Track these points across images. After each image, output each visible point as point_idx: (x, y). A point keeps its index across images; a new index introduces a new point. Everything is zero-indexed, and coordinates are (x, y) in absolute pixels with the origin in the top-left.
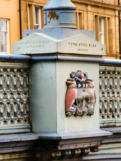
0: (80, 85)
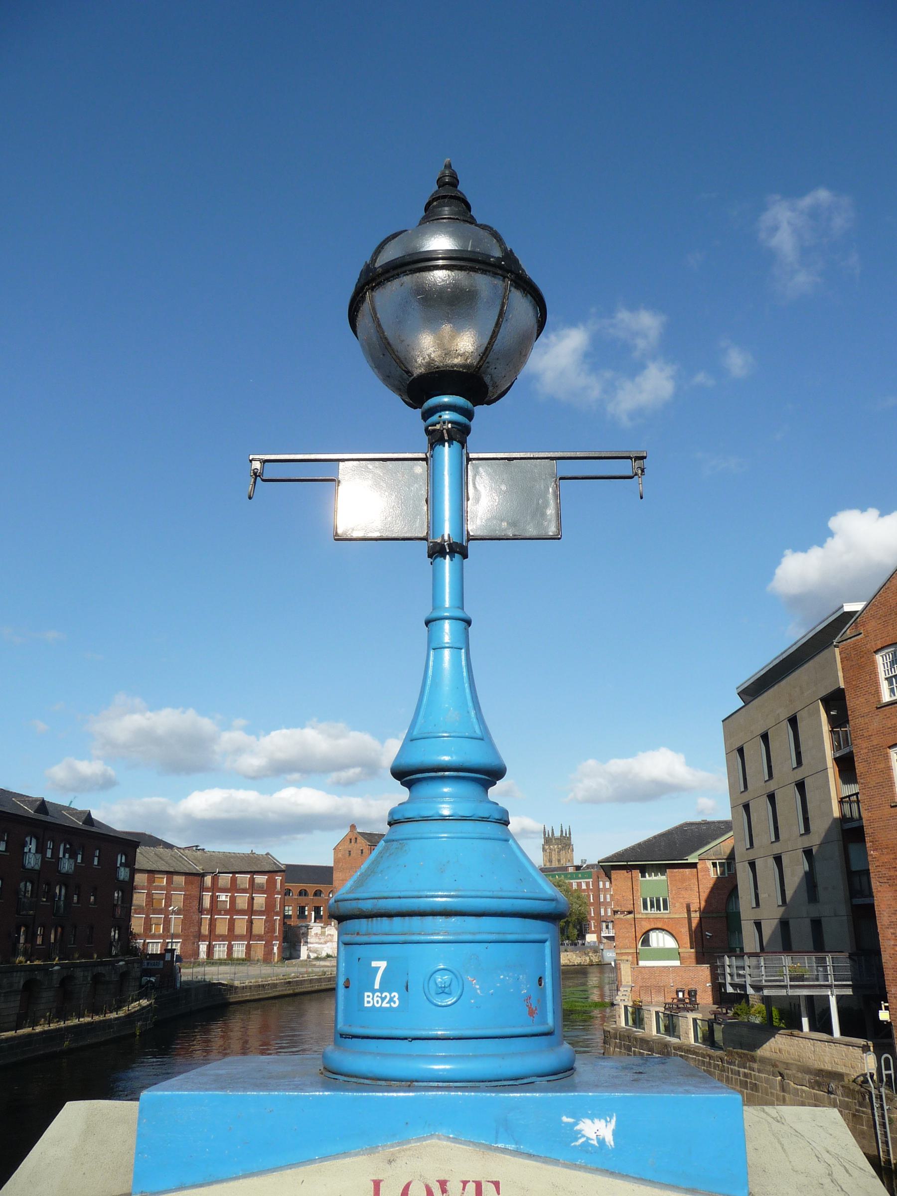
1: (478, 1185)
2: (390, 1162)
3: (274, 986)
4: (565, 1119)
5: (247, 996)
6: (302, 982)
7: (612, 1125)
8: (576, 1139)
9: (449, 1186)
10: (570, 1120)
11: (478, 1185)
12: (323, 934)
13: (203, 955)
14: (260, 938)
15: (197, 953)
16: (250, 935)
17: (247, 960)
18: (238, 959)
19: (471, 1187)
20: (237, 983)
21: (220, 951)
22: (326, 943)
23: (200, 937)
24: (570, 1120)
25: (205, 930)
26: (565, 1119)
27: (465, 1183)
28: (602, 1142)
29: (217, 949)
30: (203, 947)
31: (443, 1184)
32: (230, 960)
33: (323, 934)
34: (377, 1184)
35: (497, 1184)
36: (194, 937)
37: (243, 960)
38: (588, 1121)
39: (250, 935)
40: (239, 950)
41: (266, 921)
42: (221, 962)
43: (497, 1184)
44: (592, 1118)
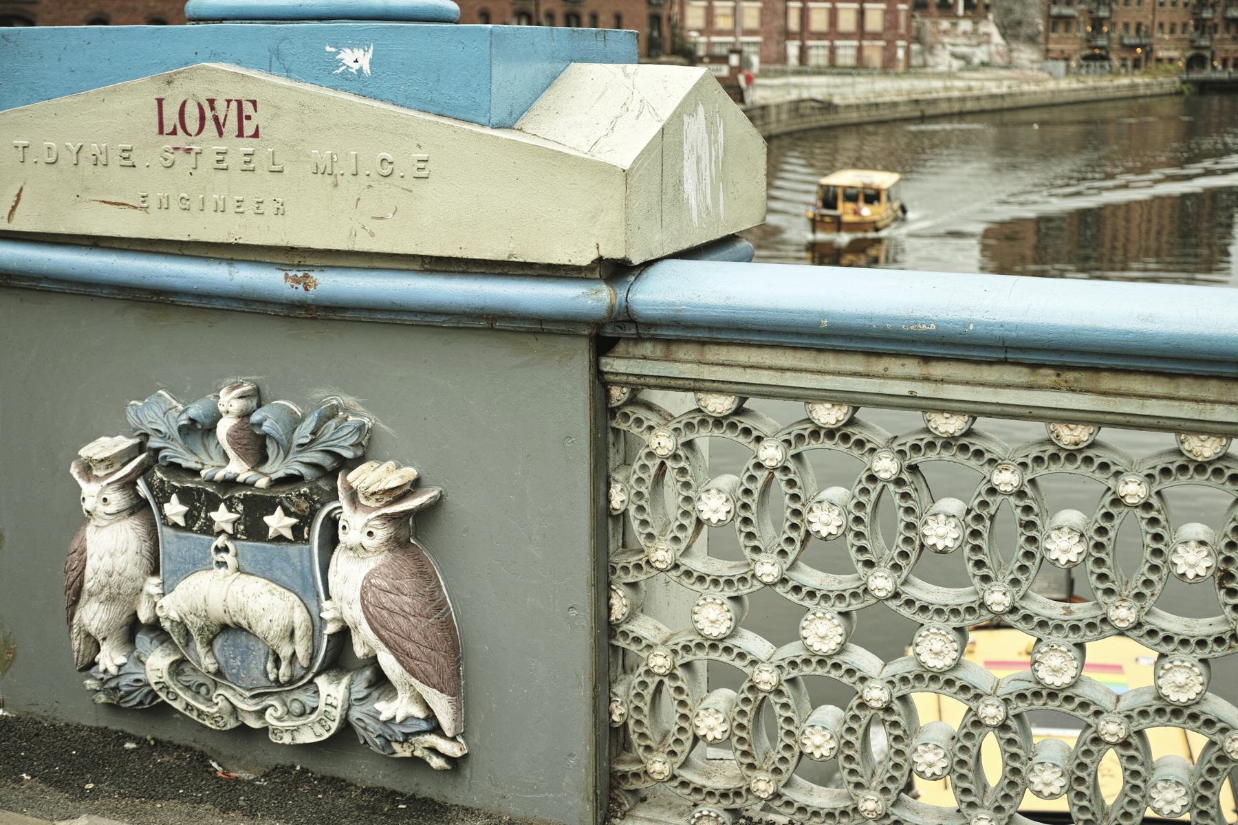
0: (175, 509)
1: (240, 103)
2: (169, 83)
3: (894, 104)
4: (328, 49)
5: (854, 116)
6: (934, 102)
7: (369, 55)
8: (338, 67)
9: (216, 104)
10: (333, 50)
11: (240, 103)
12: (975, 32)
13: (793, 60)
14: (875, 36)
15: (784, 58)
16: (861, 32)
17: (860, 66)
18: (845, 67)
19: (234, 105)
20: (837, 100)
21: (818, 55)
22: (979, 45)
23: (788, 35)
24: (333, 50)
25: (794, 24)
26: (328, 49)
27: (229, 101)
28: (360, 71)
29: (813, 52)
30: (793, 49)
31: (211, 102)
32: (832, 67)
33: (975, 32)
34: (160, 101)
35: (254, 103)
36: (780, 34)
37: (853, 68)
38: (348, 51)
39: (861, 32)
40: (846, 52)
41: (886, 12)
42: (819, 72)
43: (254, 103)
44: (351, 47)
